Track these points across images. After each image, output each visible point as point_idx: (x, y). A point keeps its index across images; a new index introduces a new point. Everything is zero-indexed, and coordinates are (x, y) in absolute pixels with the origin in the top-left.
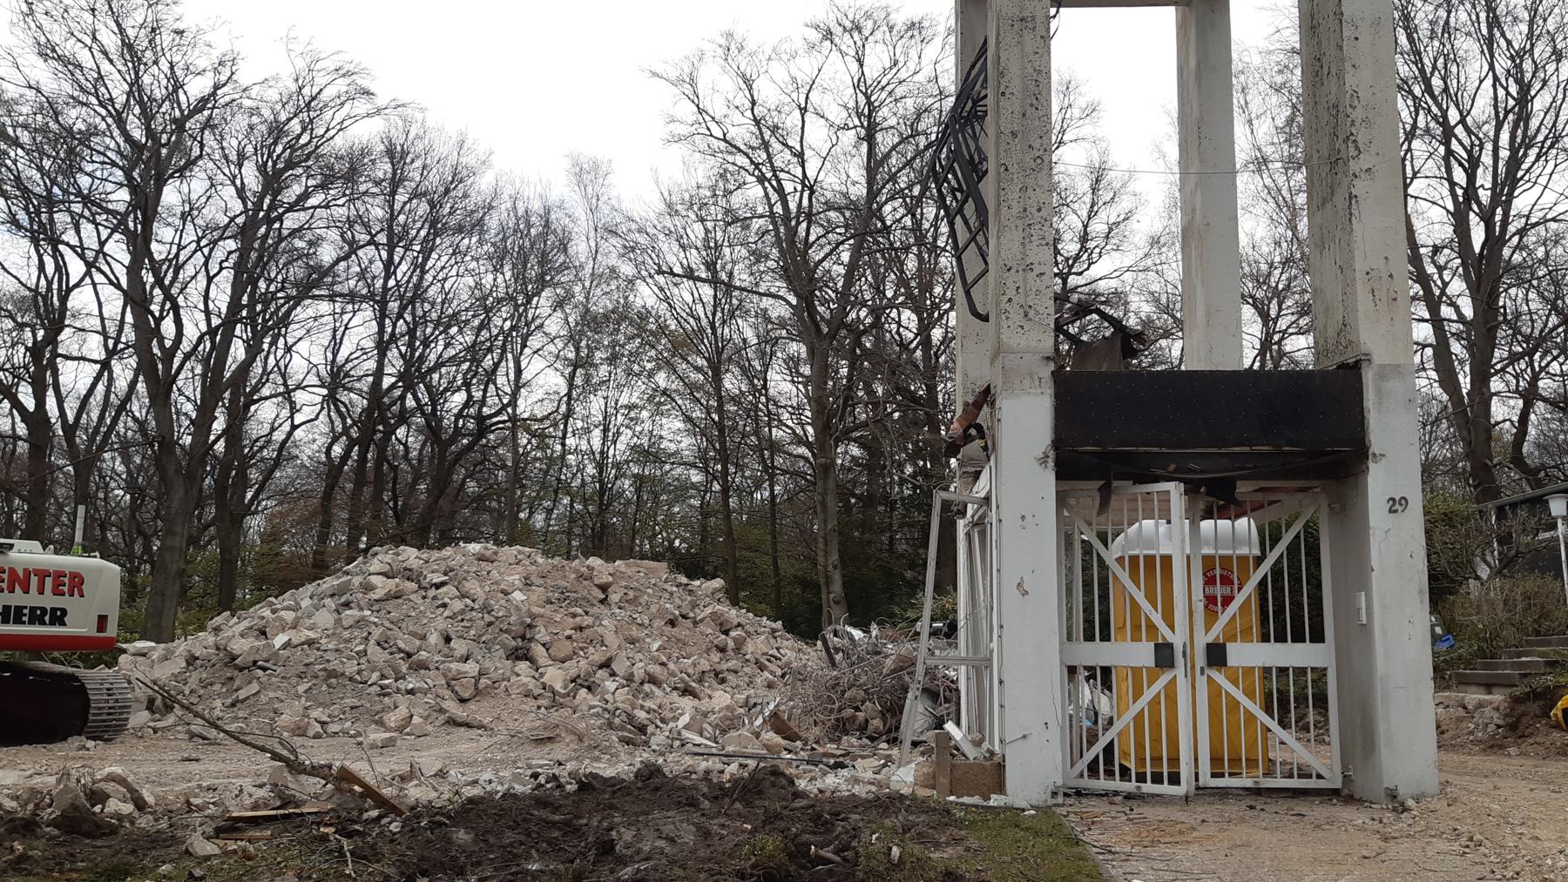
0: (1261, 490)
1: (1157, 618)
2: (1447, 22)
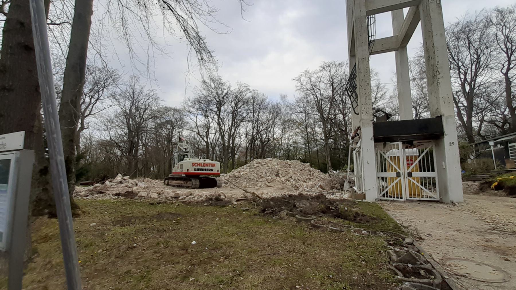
0: (418, 142)
1: (396, 168)
2: (458, 45)
